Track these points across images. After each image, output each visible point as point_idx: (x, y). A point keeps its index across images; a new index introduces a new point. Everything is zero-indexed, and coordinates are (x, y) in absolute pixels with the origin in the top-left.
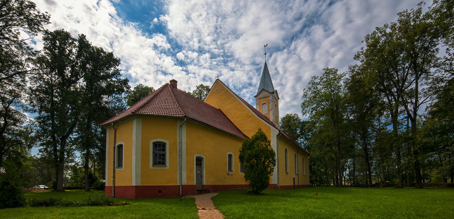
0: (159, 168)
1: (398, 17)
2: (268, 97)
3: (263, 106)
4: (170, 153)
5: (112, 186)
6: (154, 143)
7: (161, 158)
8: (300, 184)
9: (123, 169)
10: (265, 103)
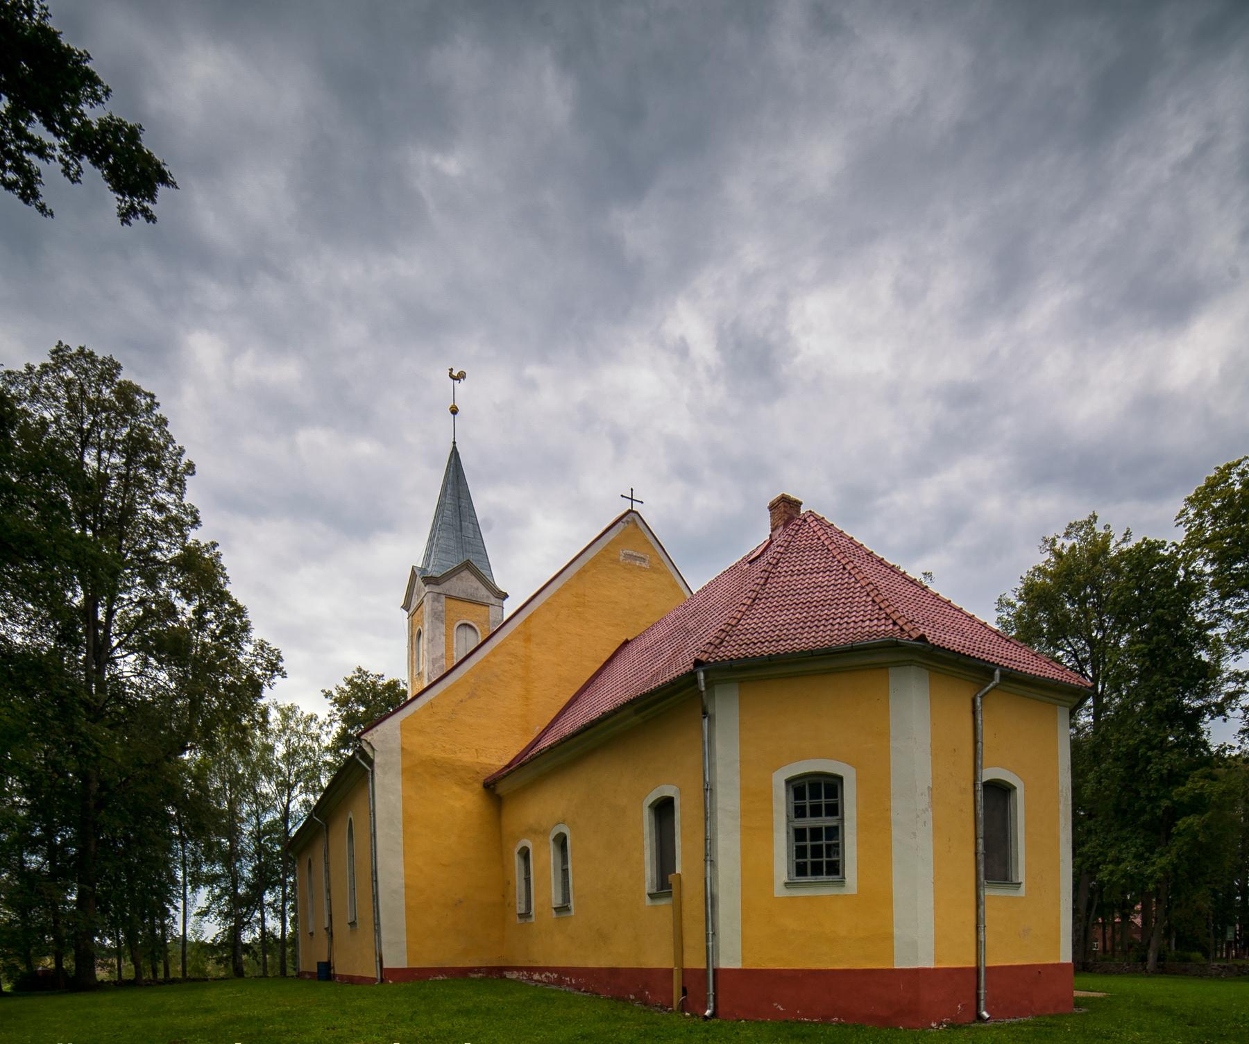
0: (819, 892)
1: (1215, 471)
2: (487, 605)
3: (460, 630)
4: (862, 827)
5: (671, 970)
6: (788, 782)
7: (828, 847)
8: (992, 960)
10: (471, 627)
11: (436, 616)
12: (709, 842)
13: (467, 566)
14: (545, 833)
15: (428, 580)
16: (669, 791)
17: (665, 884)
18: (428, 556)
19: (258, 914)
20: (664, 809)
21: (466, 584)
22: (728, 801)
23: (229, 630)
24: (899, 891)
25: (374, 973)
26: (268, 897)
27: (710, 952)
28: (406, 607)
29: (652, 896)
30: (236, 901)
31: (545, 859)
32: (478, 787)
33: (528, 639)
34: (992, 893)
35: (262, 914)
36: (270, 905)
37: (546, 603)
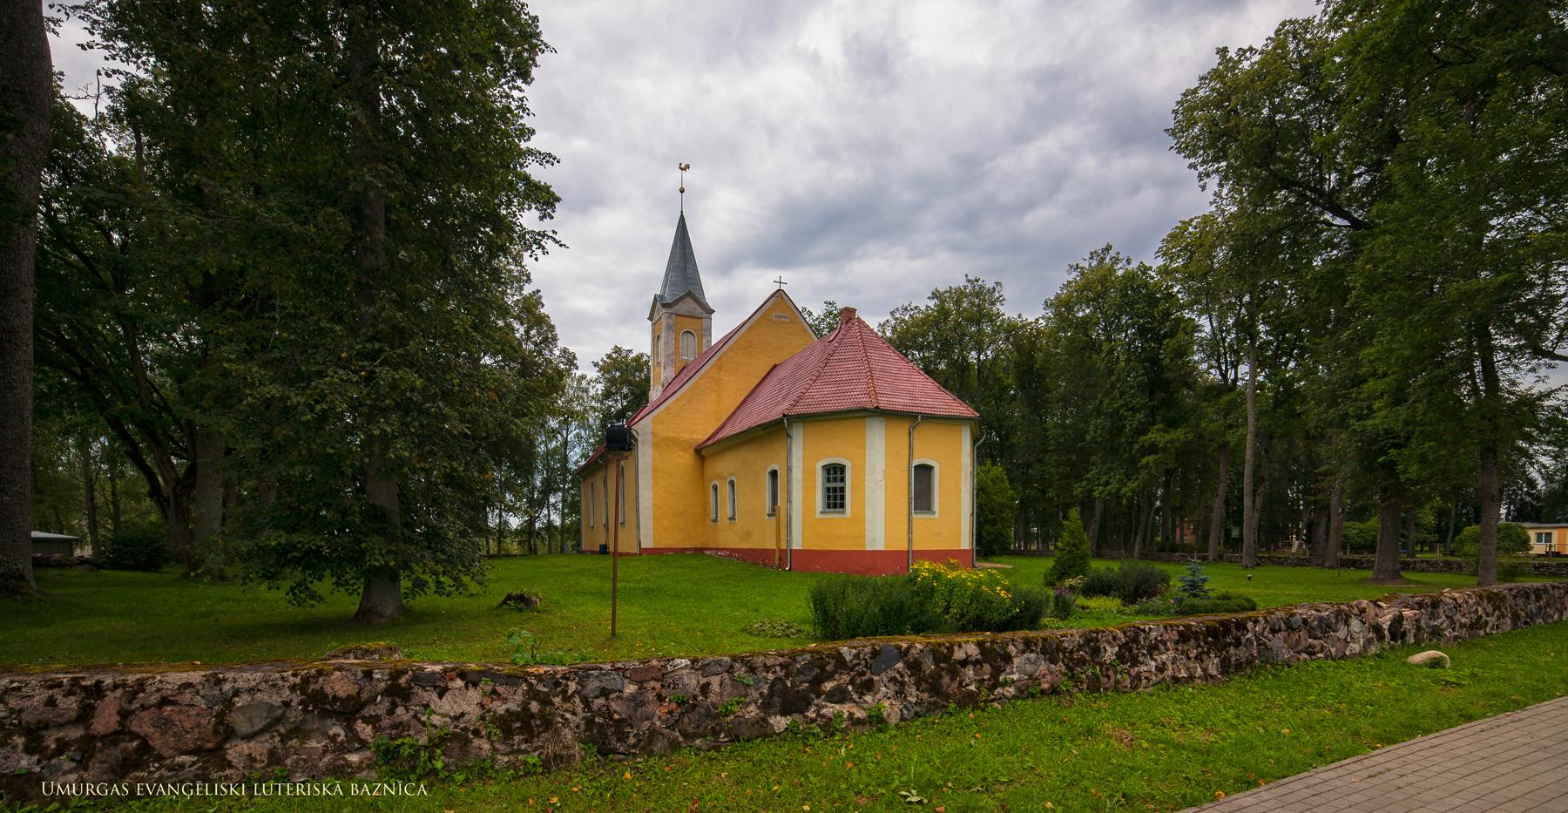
0: (835, 516)
2: (701, 318)
6: (823, 467)
8: (916, 547)
9: (937, 516)
11: (669, 327)
12: (789, 493)
13: (689, 294)
14: (725, 479)
15: (665, 306)
16: (776, 467)
17: (774, 512)
18: (664, 286)
19: (546, 512)
20: (774, 474)
21: (688, 306)
22: (797, 474)
23: (545, 340)
24: (868, 514)
25: (636, 551)
26: (552, 500)
27: (789, 542)
28: (651, 318)
29: (769, 515)
30: (531, 502)
31: (725, 491)
32: (692, 451)
33: (720, 369)
34: (919, 518)
35: (549, 511)
36: (553, 505)
37: (731, 348)
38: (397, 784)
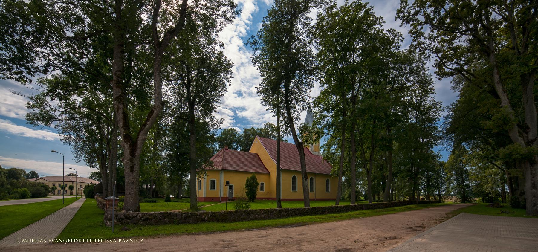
0: (213, 190)
8: (316, 198)
38: (134, 240)
